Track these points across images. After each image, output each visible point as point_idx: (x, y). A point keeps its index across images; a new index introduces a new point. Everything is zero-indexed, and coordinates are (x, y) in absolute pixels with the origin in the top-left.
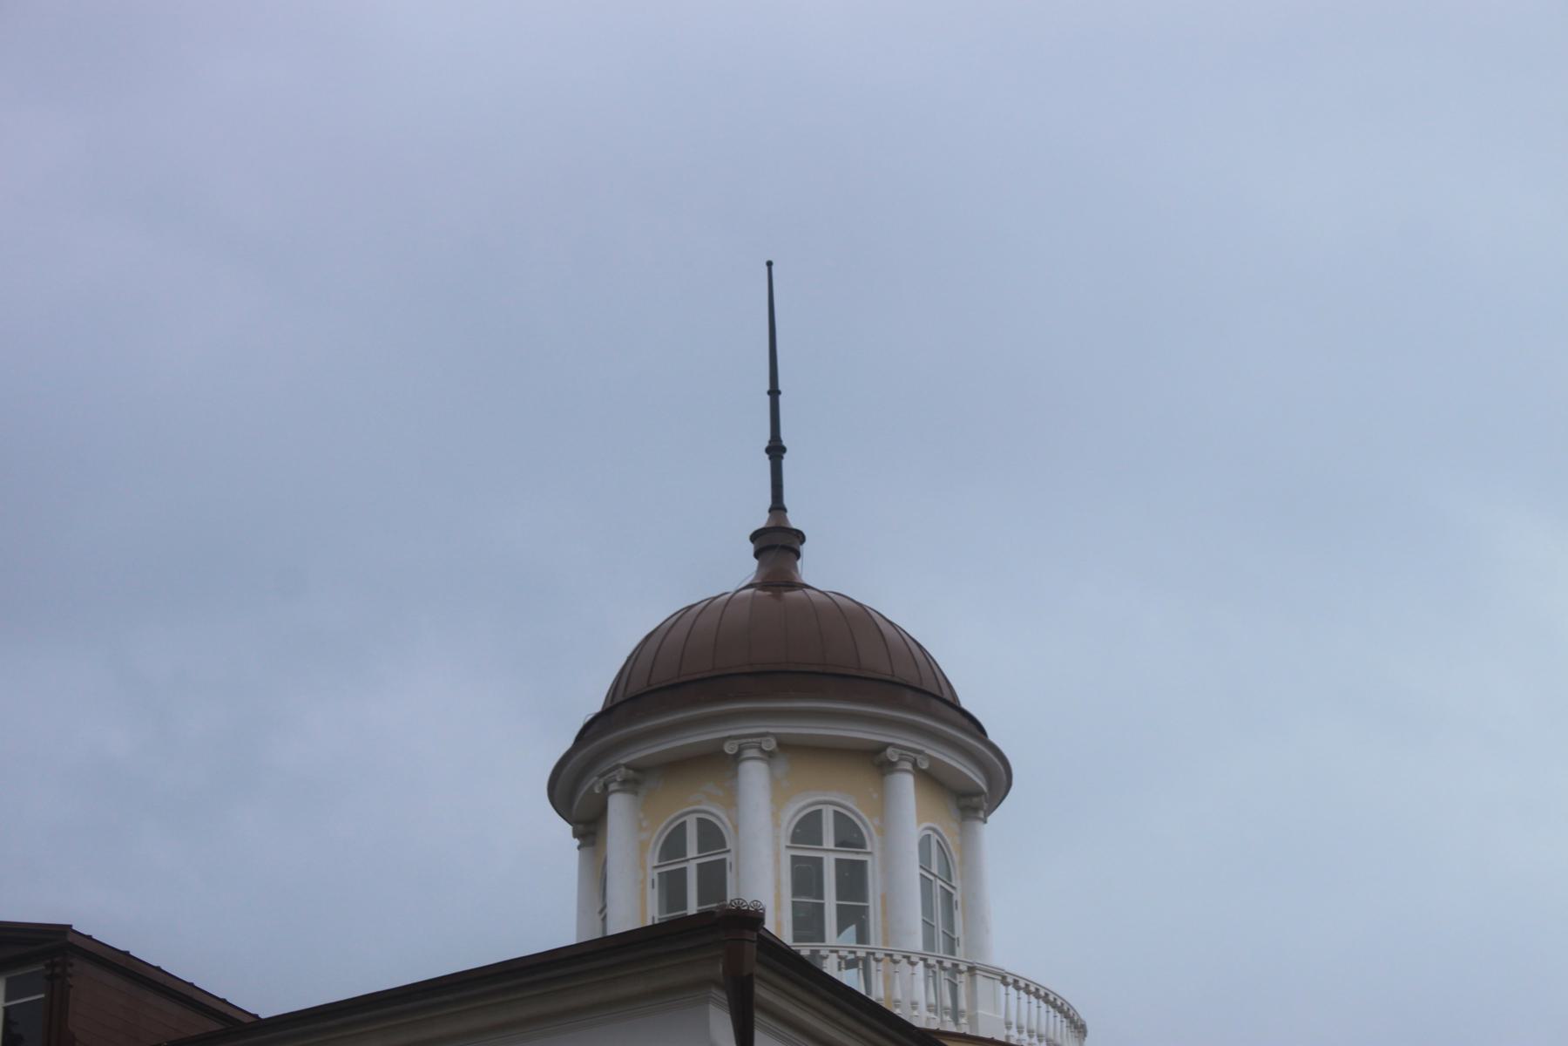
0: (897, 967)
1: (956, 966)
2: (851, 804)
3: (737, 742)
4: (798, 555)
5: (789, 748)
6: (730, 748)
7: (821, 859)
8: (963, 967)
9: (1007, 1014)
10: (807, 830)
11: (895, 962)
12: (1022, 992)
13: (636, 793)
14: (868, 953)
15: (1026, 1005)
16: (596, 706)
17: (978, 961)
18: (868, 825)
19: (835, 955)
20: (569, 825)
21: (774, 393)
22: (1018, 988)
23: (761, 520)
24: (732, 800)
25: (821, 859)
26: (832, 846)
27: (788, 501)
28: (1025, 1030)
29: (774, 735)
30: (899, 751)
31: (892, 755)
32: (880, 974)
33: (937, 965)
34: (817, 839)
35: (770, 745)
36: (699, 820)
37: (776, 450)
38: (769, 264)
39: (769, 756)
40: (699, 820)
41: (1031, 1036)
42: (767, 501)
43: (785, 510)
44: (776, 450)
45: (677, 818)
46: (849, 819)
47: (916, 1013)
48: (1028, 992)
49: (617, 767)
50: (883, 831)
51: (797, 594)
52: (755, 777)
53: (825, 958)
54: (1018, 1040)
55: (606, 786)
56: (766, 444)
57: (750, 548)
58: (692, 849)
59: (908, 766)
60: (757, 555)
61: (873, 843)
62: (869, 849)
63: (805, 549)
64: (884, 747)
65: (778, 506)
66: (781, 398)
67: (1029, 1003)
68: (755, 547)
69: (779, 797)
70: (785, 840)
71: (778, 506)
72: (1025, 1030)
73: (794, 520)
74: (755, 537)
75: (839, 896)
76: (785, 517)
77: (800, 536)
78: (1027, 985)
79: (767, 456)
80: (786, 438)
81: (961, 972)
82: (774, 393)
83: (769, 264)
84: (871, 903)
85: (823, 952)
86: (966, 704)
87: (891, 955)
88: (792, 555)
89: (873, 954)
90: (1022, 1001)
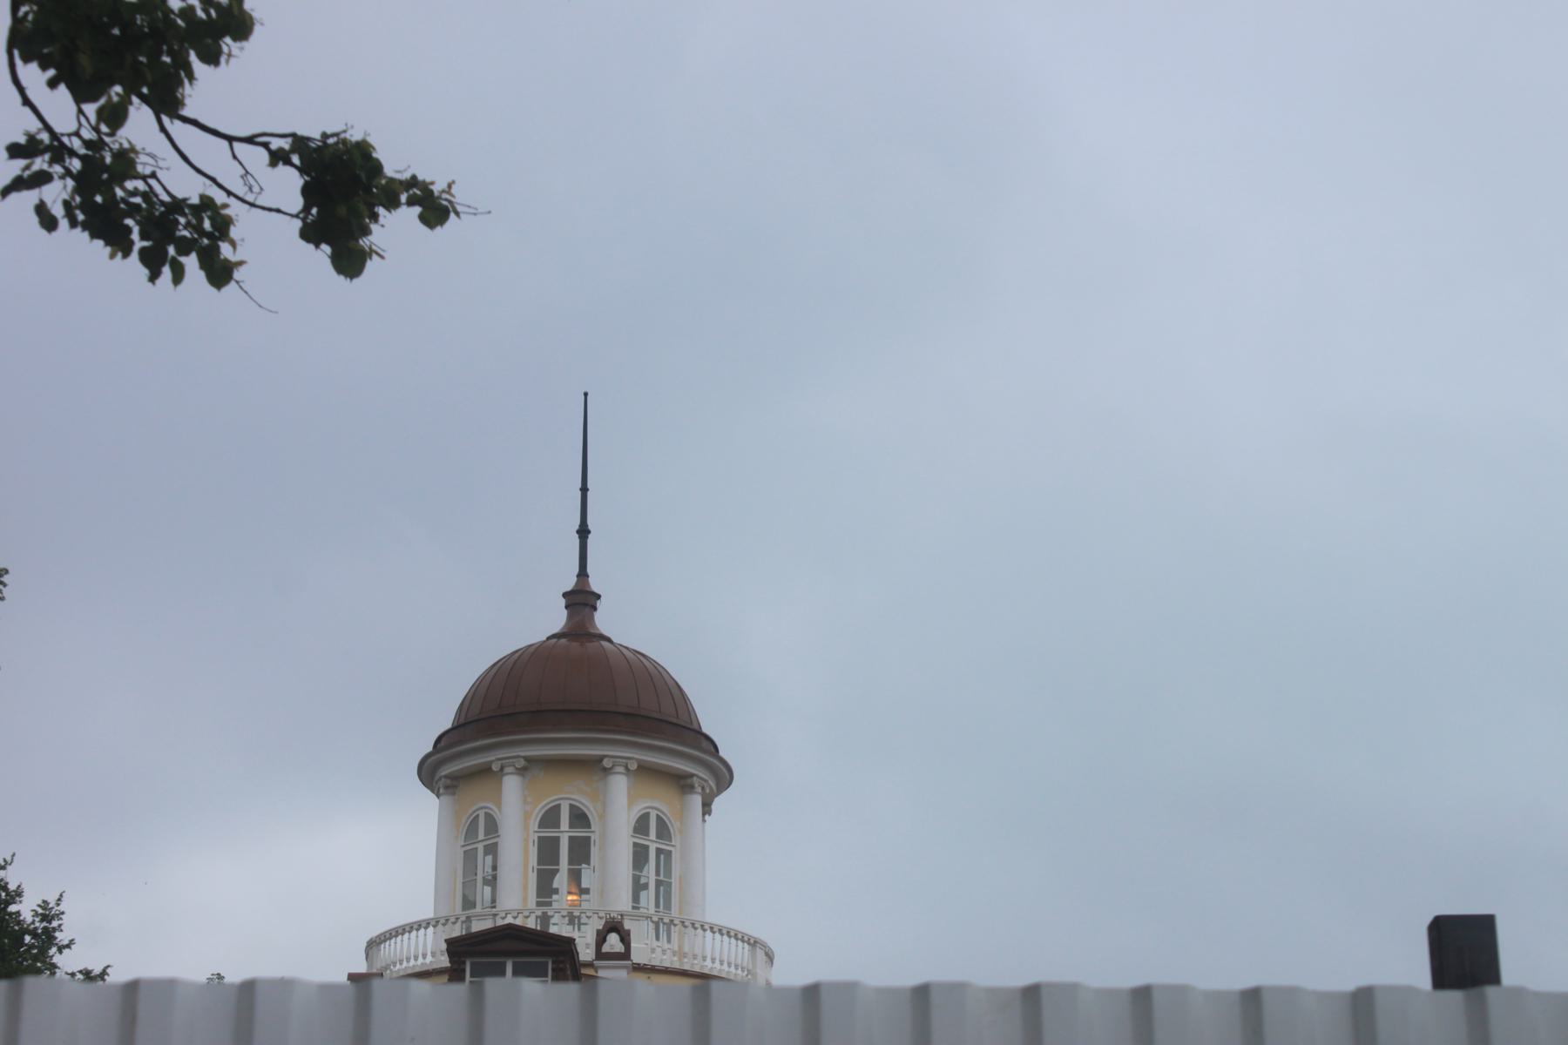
0: (687, 930)
1: (672, 921)
3: (500, 762)
4: (595, 608)
6: (495, 767)
7: (559, 837)
8: (676, 922)
9: (729, 956)
10: (550, 818)
11: (686, 927)
12: (746, 944)
13: (454, 794)
14: (581, 913)
15: (720, 943)
16: (446, 723)
17: (697, 917)
18: (674, 826)
19: (596, 915)
21: (584, 490)
22: (737, 939)
23: (570, 583)
24: (499, 805)
25: (559, 837)
26: (567, 829)
27: (591, 569)
28: (733, 965)
29: (637, 760)
30: (612, 760)
31: (607, 763)
32: (676, 934)
33: (690, 925)
34: (557, 825)
35: (633, 766)
36: (486, 813)
37: (583, 532)
38: (586, 394)
39: (522, 772)
40: (486, 813)
41: (737, 969)
42: (576, 570)
43: (588, 576)
44: (583, 532)
45: (474, 812)
46: (664, 822)
47: (696, 962)
48: (743, 941)
49: (440, 779)
50: (603, 816)
52: (619, 785)
53: (552, 916)
54: (735, 974)
55: (502, 769)
56: (577, 527)
57: (563, 602)
58: (481, 836)
59: (621, 769)
60: (566, 607)
61: (676, 840)
62: (673, 843)
63: (600, 604)
65: (583, 573)
66: (580, 486)
67: (730, 943)
68: (566, 602)
69: (631, 801)
70: (534, 824)
71: (583, 573)
72: (733, 965)
73: (595, 584)
74: (565, 595)
76: (588, 581)
78: (736, 935)
79: (577, 536)
81: (675, 925)
82: (584, 490)
83: (586, 394)
84: (673, 880)
85: (550, 914)
86: (705, 730)
87: (683, 922)
88: (587, 609)
89: (662, 919)
90: (707, 939)
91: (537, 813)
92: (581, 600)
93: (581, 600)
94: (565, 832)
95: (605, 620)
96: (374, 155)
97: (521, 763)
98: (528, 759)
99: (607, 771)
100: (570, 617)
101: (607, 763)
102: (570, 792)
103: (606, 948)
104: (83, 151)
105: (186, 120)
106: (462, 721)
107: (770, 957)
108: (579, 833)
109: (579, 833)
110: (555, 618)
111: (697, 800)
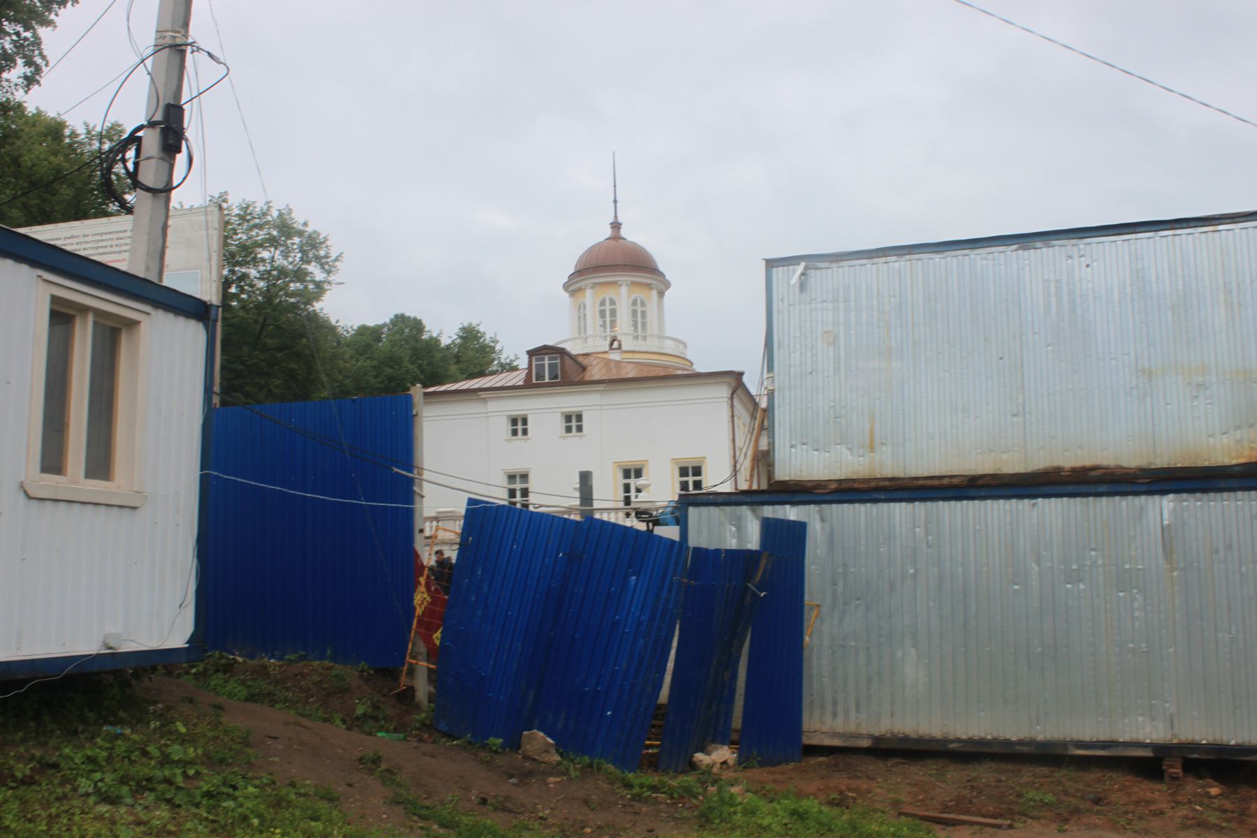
2: (613, 296)
5: (633, 283)
6: (583, 287)
18: (616, 300)
20: (148, 194)
21: (615, 186)
23: (612, 220)
27: (618, 215)
29: (98, 313)
37: (615, 201)
39: (592, 288)
42: (613, 215)
51: (621, 241)
52: (624, 289)
55: (586, 287)
61: (618, 304)
63: (622, 227)
64: (651, 284)
65: (616, 217)
70: (618, 309)
71: (616, 217)
73: (620, 220)
74: (611, 224)
75: (610, 317)
77: (621, 224)
80: (618, 199)
82: (615, 186)
83: (614, 153)
91: (598, 301)
92: (616, 226)
93: (616, 226)
94: (608, 307)
95: (624, 232)
96: (415, 488)
97: (591, 285)
98: (594, 284)
99: (620, 285)
100: (613, 231)
101: (620, 283)
102: (608, 293)
103: (105, 140)
104: (617, 791)
105: (505, 488)
106: (578, 269)
107: (685, 345)
108: (643, 309)
109: (634, 308)
110: (608, 232)
111: (654, 293)
